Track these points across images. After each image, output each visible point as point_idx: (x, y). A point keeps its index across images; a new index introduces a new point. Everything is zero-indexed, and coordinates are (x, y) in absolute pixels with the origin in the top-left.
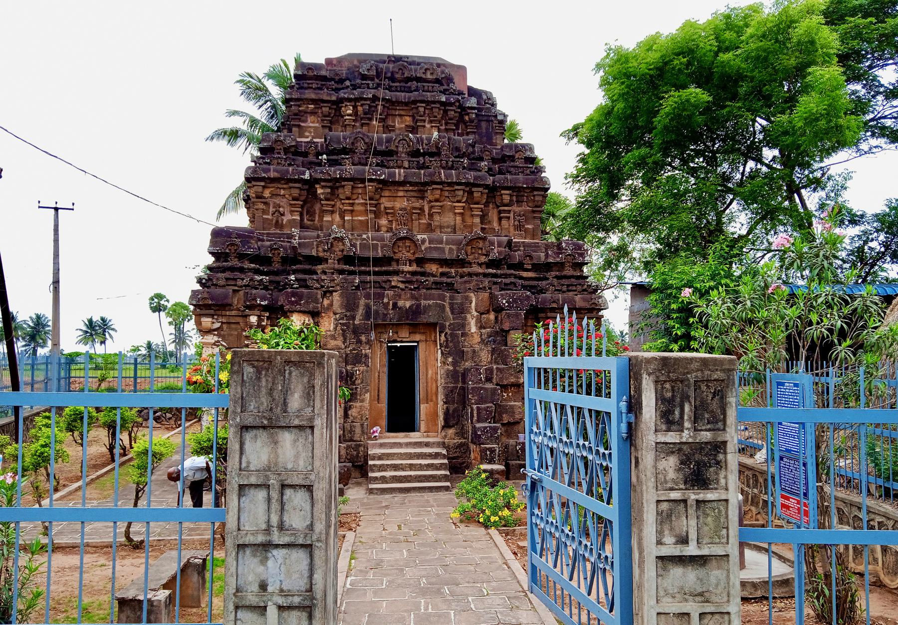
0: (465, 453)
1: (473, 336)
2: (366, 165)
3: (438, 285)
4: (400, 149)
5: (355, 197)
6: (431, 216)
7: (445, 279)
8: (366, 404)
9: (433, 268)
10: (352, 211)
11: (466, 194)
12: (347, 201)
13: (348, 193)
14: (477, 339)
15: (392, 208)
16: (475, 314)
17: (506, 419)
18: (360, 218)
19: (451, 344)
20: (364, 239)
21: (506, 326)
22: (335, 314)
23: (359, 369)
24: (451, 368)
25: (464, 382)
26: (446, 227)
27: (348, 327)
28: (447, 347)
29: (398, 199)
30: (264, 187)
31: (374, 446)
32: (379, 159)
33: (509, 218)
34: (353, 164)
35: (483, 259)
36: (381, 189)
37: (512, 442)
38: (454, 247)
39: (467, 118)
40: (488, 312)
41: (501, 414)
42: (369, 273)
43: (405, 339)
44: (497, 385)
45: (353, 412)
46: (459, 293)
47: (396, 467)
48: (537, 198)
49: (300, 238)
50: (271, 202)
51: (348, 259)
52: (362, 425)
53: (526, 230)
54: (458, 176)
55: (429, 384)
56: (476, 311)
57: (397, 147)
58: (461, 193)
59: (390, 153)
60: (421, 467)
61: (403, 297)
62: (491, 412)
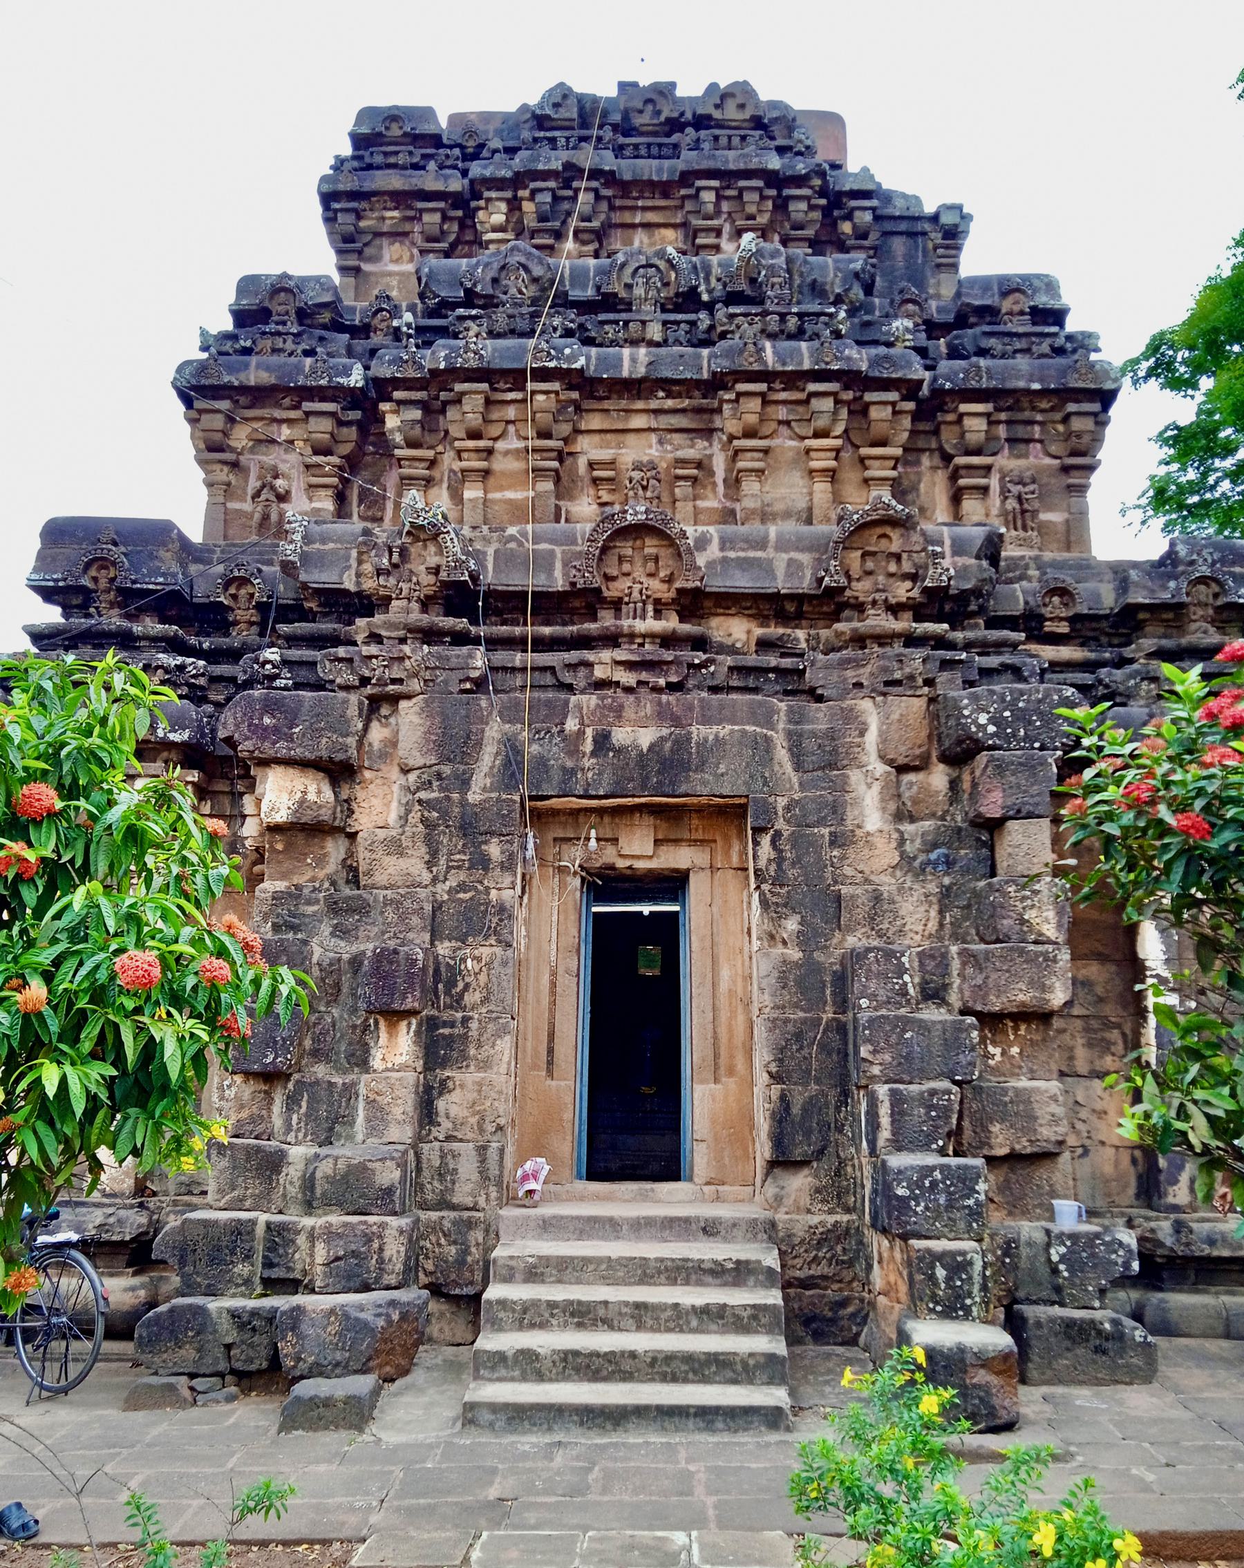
0: (850, 1264)
2: (530, 334)
3: (749, 677)
4: (639, 291)
5: (495, 430)
6: (734, 483)
7: (773, 660)
8: (500, 1076)
9: (736, 630)
10: (486, 473)
11: (844, 413)
12: (471, 444)
13: (474, 420)
14: (886, 854)
15: (611, 464)
16: (880, 768)
17: (1002, 1141)
18: (510, 495)
19: (792, 873)
20: (512, 538)
22: (406, 771)
23: (478, 957)
24: (795, 954)
25: (843, 1004)
26: (776, 508)
27: (445, 815)
28: (778, 881)
29: (631, 439)
31: (521, 1228)
32: (571, 318)
33: (985, 490)
34: (492, 334)
35: (902, 591)
36: (578, 409)
37: (1029, 1229)
38: (805, 558)
39: (846, 227)
40: (920, 765)
41: (982, 1126)
42: (517, 643)
43: (638, 849)
44: (964, 1012)
45: (451, 1106)
46: (820, 699)
47: (583, 1315)
48: (1077, 424)
49: (307, 539)
50: (252, 462)
51: (458, 596)
52: (482, 1150)
53: (1043, 529)
54: (816, 355)
55: (724, 1016)
56: (882, 757)
57: (629, 287)
58: (827, 404)
59: (608, 303)
60: (678, 1319)
61: (629, 713)
62: (947, 1110)
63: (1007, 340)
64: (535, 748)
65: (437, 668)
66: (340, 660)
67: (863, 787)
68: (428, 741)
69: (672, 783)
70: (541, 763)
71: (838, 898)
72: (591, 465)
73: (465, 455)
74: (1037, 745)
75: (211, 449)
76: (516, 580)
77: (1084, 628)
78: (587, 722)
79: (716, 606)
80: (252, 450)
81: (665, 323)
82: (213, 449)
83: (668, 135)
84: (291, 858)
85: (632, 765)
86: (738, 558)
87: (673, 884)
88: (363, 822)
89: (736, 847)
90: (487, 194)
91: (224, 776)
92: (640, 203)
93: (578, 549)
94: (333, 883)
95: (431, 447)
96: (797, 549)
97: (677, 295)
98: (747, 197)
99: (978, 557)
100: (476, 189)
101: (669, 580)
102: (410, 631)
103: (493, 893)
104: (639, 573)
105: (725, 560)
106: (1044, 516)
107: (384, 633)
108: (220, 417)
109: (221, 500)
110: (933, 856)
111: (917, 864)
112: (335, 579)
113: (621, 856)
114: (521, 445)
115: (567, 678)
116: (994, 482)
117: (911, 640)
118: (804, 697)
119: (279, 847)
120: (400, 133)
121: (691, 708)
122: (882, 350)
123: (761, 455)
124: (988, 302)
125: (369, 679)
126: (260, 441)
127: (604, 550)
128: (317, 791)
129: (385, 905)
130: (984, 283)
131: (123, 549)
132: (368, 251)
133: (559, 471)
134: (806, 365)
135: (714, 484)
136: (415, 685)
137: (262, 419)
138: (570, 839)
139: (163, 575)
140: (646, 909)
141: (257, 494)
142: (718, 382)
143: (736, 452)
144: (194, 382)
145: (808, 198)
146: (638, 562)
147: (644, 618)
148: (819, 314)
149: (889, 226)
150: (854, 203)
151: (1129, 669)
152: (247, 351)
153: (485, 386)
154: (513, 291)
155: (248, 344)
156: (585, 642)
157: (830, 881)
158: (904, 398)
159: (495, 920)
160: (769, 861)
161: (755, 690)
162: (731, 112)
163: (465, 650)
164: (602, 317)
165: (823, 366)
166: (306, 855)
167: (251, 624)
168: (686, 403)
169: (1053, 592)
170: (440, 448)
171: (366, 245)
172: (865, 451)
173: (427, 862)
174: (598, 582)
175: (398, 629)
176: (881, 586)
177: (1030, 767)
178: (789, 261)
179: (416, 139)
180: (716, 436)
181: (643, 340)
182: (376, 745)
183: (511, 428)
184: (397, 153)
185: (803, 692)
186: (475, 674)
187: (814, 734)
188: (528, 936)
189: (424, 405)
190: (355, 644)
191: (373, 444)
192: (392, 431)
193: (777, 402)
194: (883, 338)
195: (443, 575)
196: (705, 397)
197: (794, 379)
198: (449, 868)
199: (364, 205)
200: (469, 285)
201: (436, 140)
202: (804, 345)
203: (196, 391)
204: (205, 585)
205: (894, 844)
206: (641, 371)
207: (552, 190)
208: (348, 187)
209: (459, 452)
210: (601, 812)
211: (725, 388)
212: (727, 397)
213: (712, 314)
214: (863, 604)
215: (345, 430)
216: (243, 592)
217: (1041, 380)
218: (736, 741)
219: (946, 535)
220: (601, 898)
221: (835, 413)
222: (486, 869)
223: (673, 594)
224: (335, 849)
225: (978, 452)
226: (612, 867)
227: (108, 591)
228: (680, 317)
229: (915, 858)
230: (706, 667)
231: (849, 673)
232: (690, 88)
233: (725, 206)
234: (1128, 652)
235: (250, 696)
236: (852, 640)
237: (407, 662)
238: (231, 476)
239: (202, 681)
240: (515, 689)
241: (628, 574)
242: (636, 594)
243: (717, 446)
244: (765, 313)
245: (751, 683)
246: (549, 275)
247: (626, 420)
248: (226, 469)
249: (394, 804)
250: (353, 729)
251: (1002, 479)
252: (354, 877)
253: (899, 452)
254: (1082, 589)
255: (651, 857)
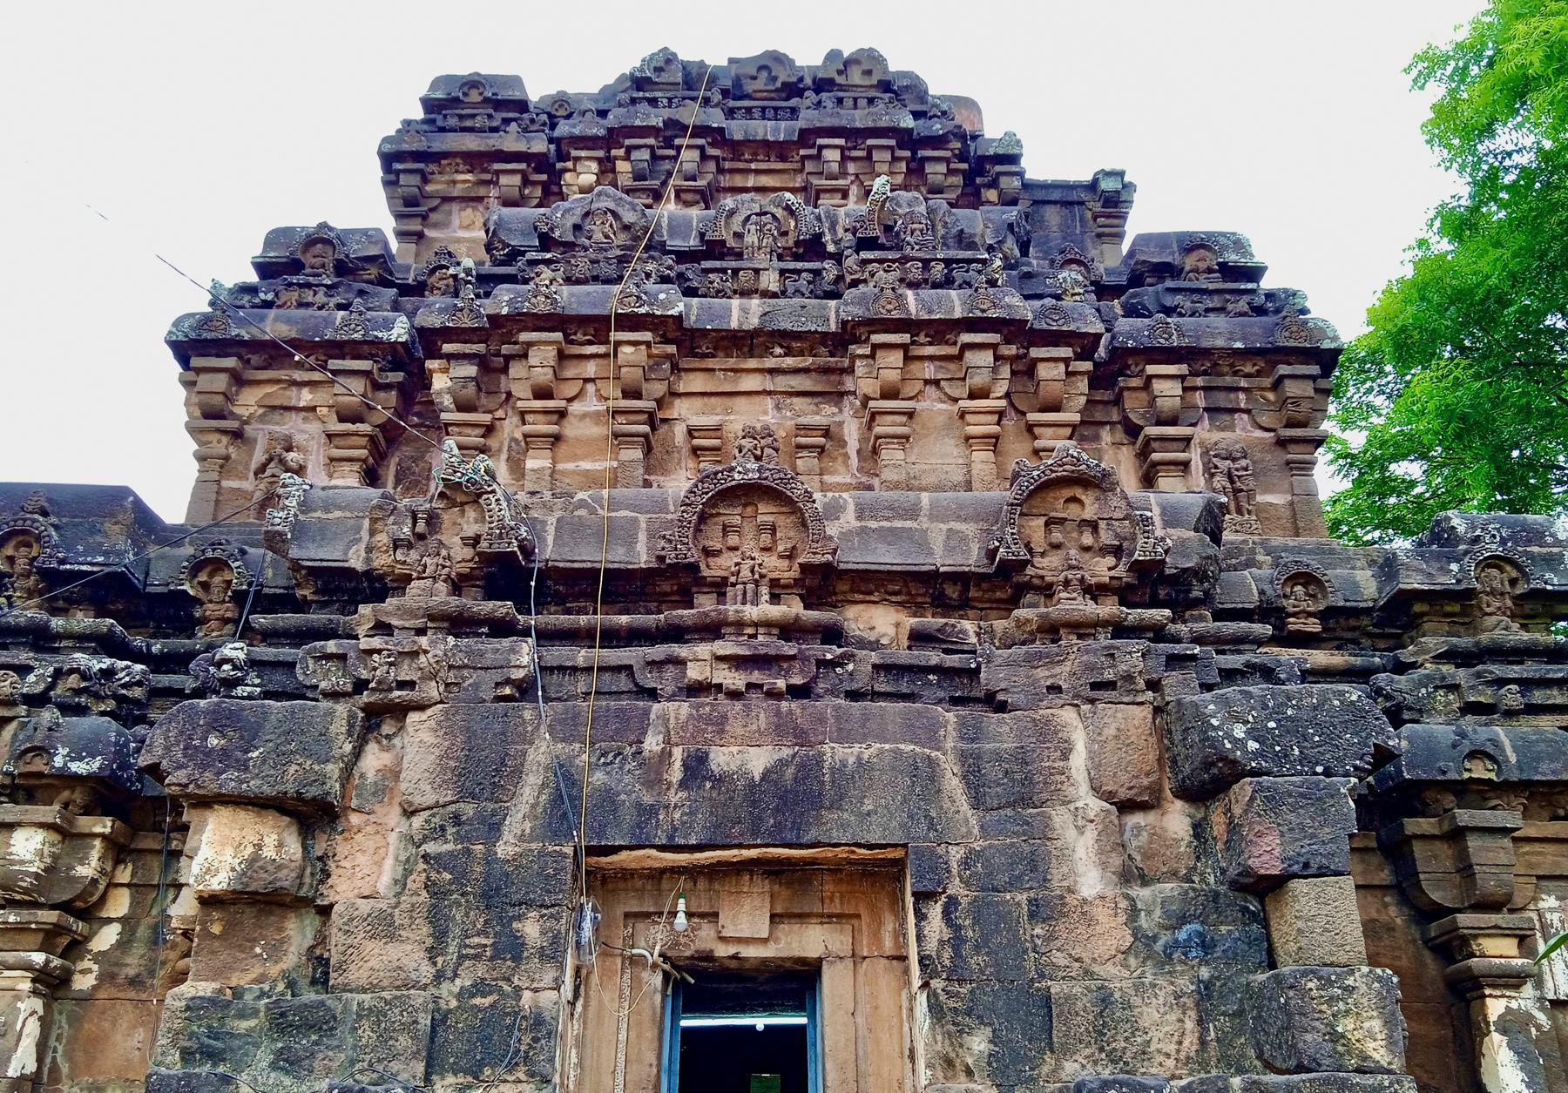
1: (1091, 921)
3: (900, 679)
4: (751, 239)
5: (571, 389)
6: (871, 453)
7: (934, 657)
9: (881, 623)
10: (557, 438)
11: (1006, 371)
12: (539, 404)
13: (543, 375)
14: (1110, 933)
16: (1095, 805)
18: (586, 465)
19: (976, 961)
20: (582, 504)
21: (1267, 855)
22: (409, 813)
27: (461, 877)
29: (740, 402)
30: (239, 380)
33: (1185, 465)
34: (569, 280)
35: (1102, 569)
38: (969, 529)
43: (747, 929)
46: (1002, 707)
48: (1292, 389)
51: (504, 573)
53: (1262, 512)
56: (1096, 790)
58: (986, 358)
61: (735, 727)
63: (1195, 297)
64: (599, 777)
65: (466, 667)
66: (329, 657)
67: (1071, 833)
68: (444, 769)
69: (797, 827)
70: (608, 798)
71: (1047, 1001)
72: (691, 432)
73: (528, 418)
74: (1319, 769)
75: (207, 415)
76: (587, 555)
77: (1340, 624)
78: (674, 739)
79: (853, 591)
80: (262, 419)
81: (782, 272)
82: (212, 417)
83: (788, 99)
84: (230, 947)
85: (738, 800)
86: (881, 529)
87: (797, 983)
88: (342, 890)
89: (889, 925)
90: (574, 153)
91: (157, 828)
92: (753, 166)
93: (670, 517)
94: (291, 985)
95: (490, 412)
96: (959, 518)
97: (797, 243)
98: (876, 156)
99: (1196, 530)
100: (563, 149)
101: (790, 555)
102: (432, 618)
103: (527, 995)
104: (749, 545)
105: (863, 530)
106: (1260, 498)
107: (395, 622)
108: (224, 377)
109: (215, 476)
110: (1182, 935)
111: (1159, 947)
112: (337, 555)
113: (723, 939)
114: (601, 407)
115: (649, 680)
116: (1195, 456)
117: (1121, 630)
118: (978, 707)
119: (216, 929)
120: (480, 99)
121: (822, 720)
122: (1049, 302)
123: (904, 419)
124: (1169, 259)
125: (368, 682)
126: (273, 408)
127: (703, 518)
128: (277, 843)
129: (360, 1017)
130: (1162, 240)
131: (53, 519)
132: (433, 217)
133: (648, 435)
134: (958, 314)
135: (846, 456)
136: (432, 690)
137: (278, 381)
138: (647, 915)
139: (106, 554)
140: (760, 1022)
141: (262, 469)
142: (845, 337)
143: (873, 416)
144: (193, 335)
145: (947, 161)
146: (749, 529)
147: (755, 602)
148: (969, 261)
149: (1040, 195)
150: (998, 168)
151: (1416, 674)
152: (268, 305)
153: (558, 336)
154: (598, 236)
155: (270, 297)
156: (676, 634)
157: (1033, 974)
158: (1079, 357)
159: (527, 1039)
160: (941, 941)
161: (909, 697)
162: (855, 77)
163: (506, 642)
164: (706, 264)
165: (979, 314)
166: (254, 941)
167: (226, 621)
168: (809, 361)
169: (1295, 579)
170: (500, 414)
171: (432, 210)
172: (1033, 417)
173: (430, 950)
174: (694, 556)
175: (416, 617)
176: (1073, 561)
177: (1314, 799)
178: (931, 212)
179: (499, 104)
180: (846, 401)
181: (756, 291)
182: (371, 777)
183: (590, 388)
184: (473, 116)
185: (977, 700)
186: (518, 674)
187: (998, 757)
188: (580, 1064)
189: (482, 361)
190: (356, 637)
191: (419, 415)
192: (439, 393)
193: (921, 358)
194: (1048, 291)
195: (484, 545)
196: (832, 355)
197: (941, 330)
198: (462, 958)
199: (432, 167)
200: (545, 229)
201: (522, 106)
202: (953, 293)
203: (191, 347)
204: (165, 571)
205: (1122, 918)
206: (753, 322)
207: (651, 147)
208: (415, 147)
209: (522, 414)
210: (693, 872)
211: (857, 341)
212: (860, 352)
213: (839, 263)
214: (1051, 585)
215: (382, 395)
216: (217, 579)
217: (1243, 339)
218: (886, 765)
219: (1153, 501)
220: (692, 1008)
221: (995, 370)
222: (517, 959)
223: (795, 573)
224: (298, 933)
225: (1173, 422)
226: (708, 957)
227: (27, 575)
228: (799, 265)
229: (1155, 938)
230: (841, 665)
231: (1041, 673)
232: (808, 56)
233: (851, 168)
234: (1406, 655)
235: (192, 707)
236: (1040, 630)
237: (422, 658)
238: (231, 449)
239: (137, 693)
240: (576, 697)
241: (736, 549)
242: (745, 573)
243: (847, 412)
244: (905, 260)
245: (904, 688)
246: (643, 222)
247: (735, 381)
248: (225, 440)
249: (389, 863)
250: (336, 752)
251: (1205, 453)
252: (321, 969)
253: (1077, 418)
254: (1335, 575)
255: (765, 941)
